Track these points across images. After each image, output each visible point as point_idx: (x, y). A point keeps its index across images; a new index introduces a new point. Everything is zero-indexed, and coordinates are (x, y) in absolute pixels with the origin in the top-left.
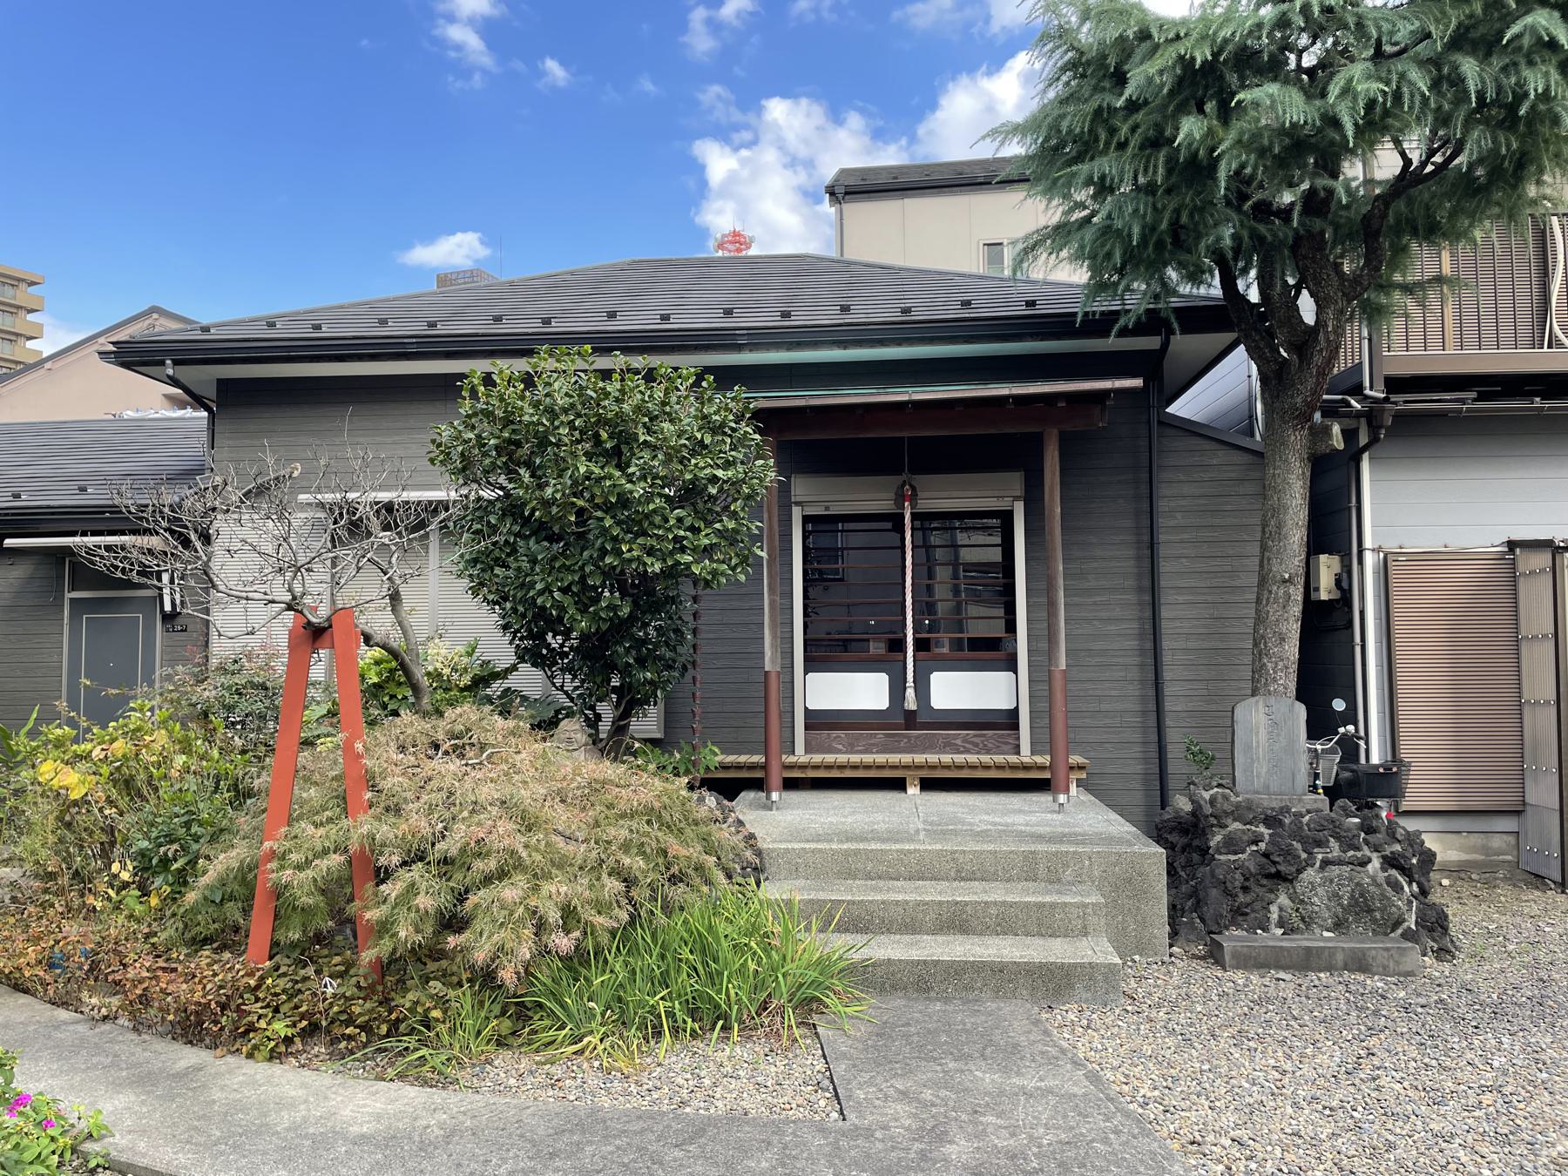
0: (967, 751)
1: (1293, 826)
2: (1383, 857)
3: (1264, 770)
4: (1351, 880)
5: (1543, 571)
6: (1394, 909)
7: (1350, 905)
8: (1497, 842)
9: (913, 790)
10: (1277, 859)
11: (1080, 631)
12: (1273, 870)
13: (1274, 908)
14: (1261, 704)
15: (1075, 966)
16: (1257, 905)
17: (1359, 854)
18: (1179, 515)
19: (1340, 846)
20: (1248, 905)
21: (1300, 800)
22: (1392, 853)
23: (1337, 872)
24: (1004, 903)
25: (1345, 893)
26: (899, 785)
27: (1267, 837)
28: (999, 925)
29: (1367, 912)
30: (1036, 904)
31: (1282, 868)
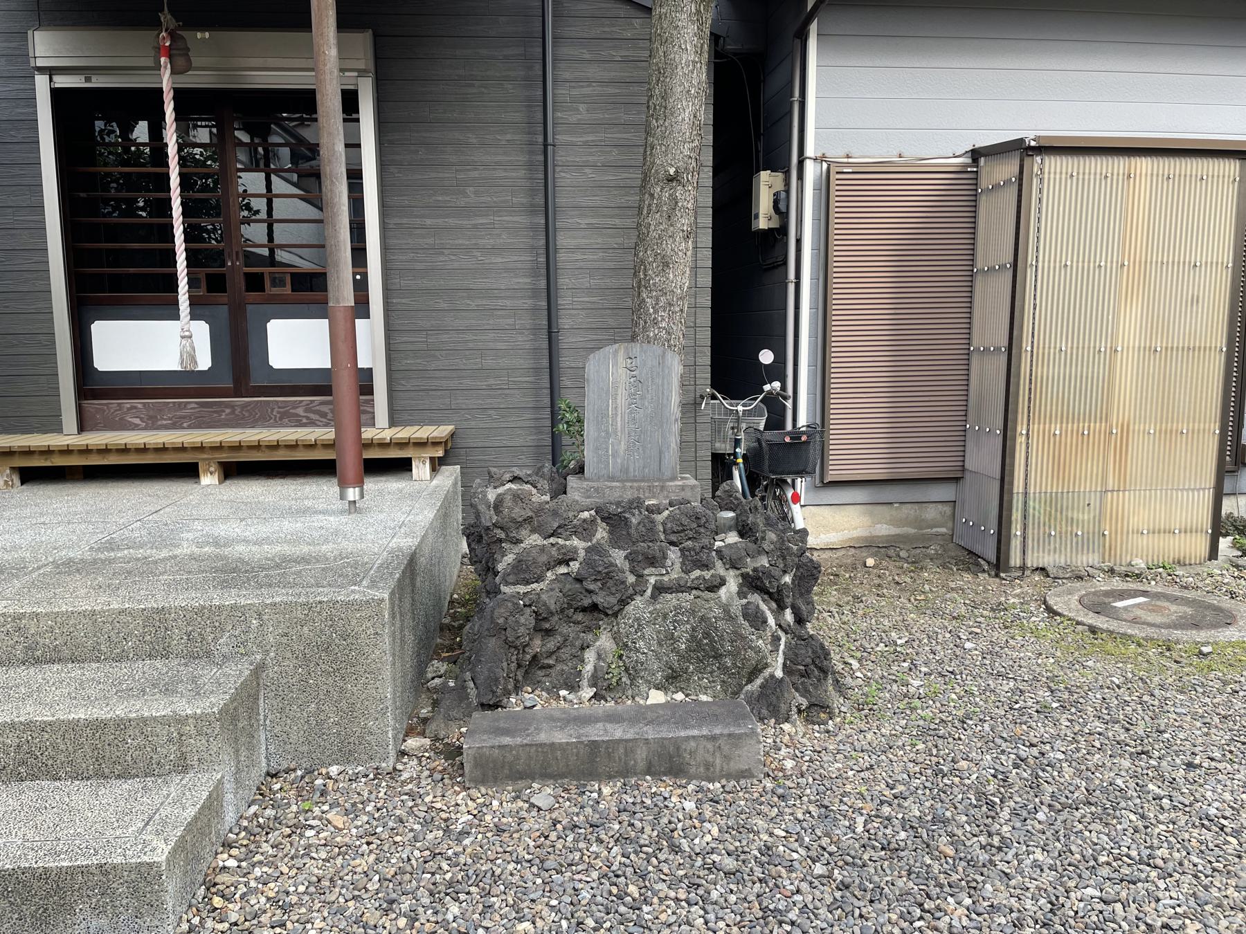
0: (312, 423)
1: (641, 527)
2: (742, 575)
3: (623, 446)
4: (693, 612)
5: (1007, 182)
6: (750, 653)
7: (689, 649)
8: (931, 513)
9: (209, 480)
10: (591, 587)
11: (456, 265)
12: (586, 602)
13: (590, 656)
14: (621, 354)
15: (71, 872)
16: (565, 653)
17: (707, 575)
18: (582, 107)
19: (683, 564)
20: (550, 655)
21: (663, 488)
22: (755, 570)
23: (675, 602)
24: (28, 725)
25: (683, 634)
26: (188, 471)
27: (582, 553)
28: (24, 763)
29: (715, 657)
30: (88, 724)
31: (599, 599)
